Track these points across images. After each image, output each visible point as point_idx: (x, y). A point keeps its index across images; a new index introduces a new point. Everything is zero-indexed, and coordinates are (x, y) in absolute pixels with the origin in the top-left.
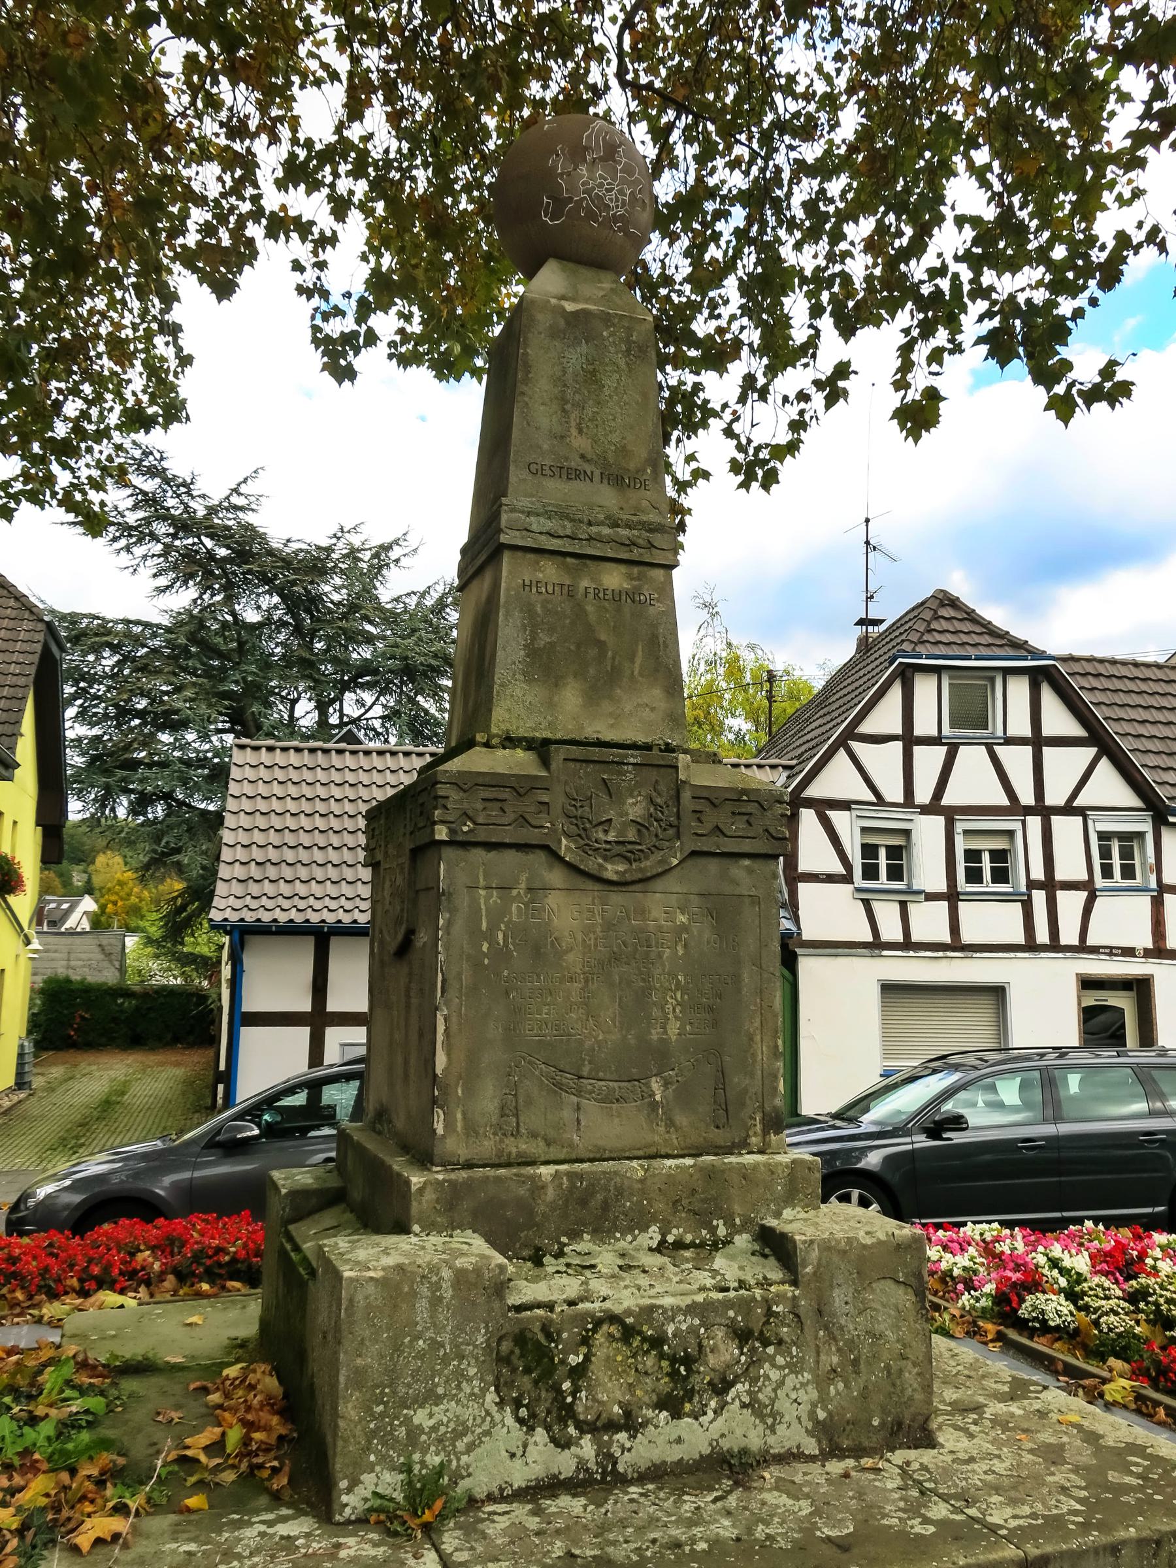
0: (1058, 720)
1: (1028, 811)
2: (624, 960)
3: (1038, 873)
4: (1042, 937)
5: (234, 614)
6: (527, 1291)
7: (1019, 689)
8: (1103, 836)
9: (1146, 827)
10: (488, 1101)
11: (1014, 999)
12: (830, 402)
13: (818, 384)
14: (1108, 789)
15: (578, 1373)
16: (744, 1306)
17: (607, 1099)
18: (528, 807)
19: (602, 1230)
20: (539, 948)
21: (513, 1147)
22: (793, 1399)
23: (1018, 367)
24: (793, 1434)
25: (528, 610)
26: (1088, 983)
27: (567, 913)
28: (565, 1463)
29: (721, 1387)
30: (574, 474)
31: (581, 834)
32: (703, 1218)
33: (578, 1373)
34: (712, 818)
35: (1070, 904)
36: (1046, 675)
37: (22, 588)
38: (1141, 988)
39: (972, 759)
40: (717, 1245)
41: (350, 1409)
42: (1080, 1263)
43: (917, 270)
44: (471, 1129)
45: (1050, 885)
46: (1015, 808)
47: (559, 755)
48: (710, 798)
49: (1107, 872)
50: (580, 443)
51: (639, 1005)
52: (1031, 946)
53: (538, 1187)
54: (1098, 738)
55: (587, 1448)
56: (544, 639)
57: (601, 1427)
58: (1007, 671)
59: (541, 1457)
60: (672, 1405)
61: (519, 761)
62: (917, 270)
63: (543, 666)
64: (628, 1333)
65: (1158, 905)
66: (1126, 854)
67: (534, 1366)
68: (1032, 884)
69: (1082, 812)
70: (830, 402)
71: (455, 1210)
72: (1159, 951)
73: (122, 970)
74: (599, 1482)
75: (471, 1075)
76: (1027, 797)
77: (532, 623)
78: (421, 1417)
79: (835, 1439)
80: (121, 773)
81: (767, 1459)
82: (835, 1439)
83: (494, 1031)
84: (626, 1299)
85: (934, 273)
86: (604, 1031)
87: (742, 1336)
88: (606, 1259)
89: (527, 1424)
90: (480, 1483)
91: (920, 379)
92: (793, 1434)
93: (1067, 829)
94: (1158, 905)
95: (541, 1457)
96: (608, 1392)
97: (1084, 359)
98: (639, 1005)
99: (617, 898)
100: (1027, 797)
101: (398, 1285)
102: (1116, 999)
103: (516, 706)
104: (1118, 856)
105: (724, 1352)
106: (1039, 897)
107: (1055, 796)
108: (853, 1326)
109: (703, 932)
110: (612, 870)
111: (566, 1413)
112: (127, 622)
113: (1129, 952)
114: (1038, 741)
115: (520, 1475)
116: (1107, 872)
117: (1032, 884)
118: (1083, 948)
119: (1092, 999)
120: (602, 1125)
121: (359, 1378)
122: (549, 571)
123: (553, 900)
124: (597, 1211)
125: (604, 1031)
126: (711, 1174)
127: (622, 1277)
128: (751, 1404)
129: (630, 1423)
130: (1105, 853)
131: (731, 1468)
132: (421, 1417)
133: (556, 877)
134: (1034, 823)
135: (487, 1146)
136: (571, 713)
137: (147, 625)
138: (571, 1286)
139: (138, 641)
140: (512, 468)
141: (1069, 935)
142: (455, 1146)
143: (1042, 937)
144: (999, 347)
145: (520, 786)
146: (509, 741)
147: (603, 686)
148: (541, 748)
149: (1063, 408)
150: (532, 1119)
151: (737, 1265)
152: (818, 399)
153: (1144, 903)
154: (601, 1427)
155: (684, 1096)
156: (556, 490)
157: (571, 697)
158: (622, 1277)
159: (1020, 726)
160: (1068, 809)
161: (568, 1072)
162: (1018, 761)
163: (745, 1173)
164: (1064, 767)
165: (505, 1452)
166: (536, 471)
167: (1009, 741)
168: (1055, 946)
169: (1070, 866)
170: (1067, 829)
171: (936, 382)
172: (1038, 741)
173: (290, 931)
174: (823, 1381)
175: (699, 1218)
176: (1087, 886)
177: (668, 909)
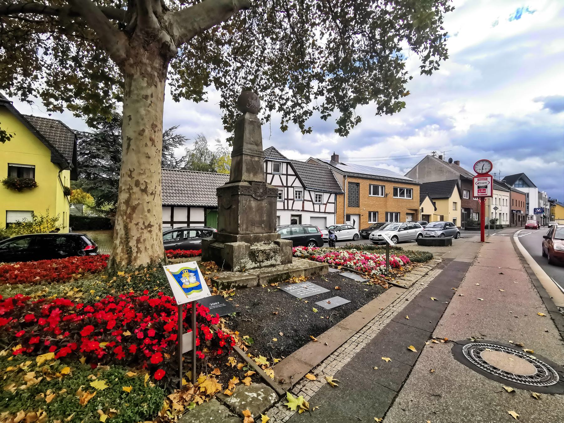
0: (290, 172)
1: (285, 187)
2: (260, 209)
3: (286, 197)
4: (286, 208)
5: (113, 133)
6: (251, 248)
7: (285, 165)
8: (296, 191)
9: (302, 190)
10: (244, 227)
11: (281, 218)
12: (267, 121)
13: (265, 118)
14: (297, 183)
15: (258, 256)
16: (274, 249)
17: (258, 227)
18: (249, 190)
19: (258, 242)
20: (250, 208)
21: (247, 232)
22: (279, 259)
23: (297, 124)
24: (279, 262)
25: (246, 163)
26: (292, 216)
27: (253, 204)
28: (256, 266)
29: (272, 258)
30: (251, 144)
31: (255, 193)
32: (268, 240)
33: (258, 256)
34: (270, 192)
35: (291, 202)
36: (289, 163)
37: (67, 125)
38: (300, 216)
39: (277, 177)
40: (270, 243)
41: (235, 260)
42: (301, 249)
43: (285, 107)
44: (243, 230)
45: (288, 199)
46: (283, 186)
47: (253, 183)
48: (270, 189)
49: (296, 197)
50: (252, 139)
51: (261, 216)
52: (284, 209)
53: (251, 237)
54: (296, 175)
55: (258, 264)
56: (248, 167)
57: (260, 262)
58: (283, 162)
59: (254, 265)
60: (267, 260)
61: (246, 184)
62: (285, 107)
63: (248, 171)
64: (263, 252)
65: (303, 202)
66: (299, 194)
67: (253, 255)
68: (285, 199)
69: (293, 187)
70: (267, 121)
71: (243, 239)
72: (303, 210)
73: (82, 213)
74: (260, 267)
75: (243, 224)
76: (285, 184)
77: (247, 165)
78: (242, 261)
79: (283, 263)
80: (85, 168)
81: (276, 265)
82: (283, 263)
83: (245, 218)
84: (262, 248)
85: (287, 108)
86: (257, 219)
87: (274, 252)
88: (258, 245)
89: (252, 262)
90: (248, 267)
91: (285, 124)
92: (279, 262)
93: (291, 190)
94: (303, 202)
95: (254, 265)
96: (261, 258)
97: (306, 125)
98: (261, 216)
99: (259, 202)
100: (285, 184)
101: (239, 247)
102: (297, 218)
103: (245, 176)
104: (298, 194)
105: (272, 254)
106: (286, 201)
107: (289, 185)
108: (285, 251)
109: (268, 206)
110: (259, 198)
111: (256, 260)
112: (84, 132)
113: (299, 210)
114: (287, 175)
115: (252, 267)
116: (296, 197)
117: (285, 199)
118: (292, 210)
119: (293, 218)
120: (257, 230)
121: (235, 256)
122: (249, 158)
123: (252, 202)
124: (257, 239)
125: (257, 219)
126: (269, 235)
127: (259, 246)
128: (275, 260)
129: (263, 262)
130: (296, 194)
131: (273, 266)
132: (242, 261)
133: (252, 199)
134: (286, 189)
135: (244, 232)
136: (252, 177)
137: (89, 133)
138: (256, 247)
139: (87, 137)
140: (244, 144)
141: (290, 208)
142: (241, 232)
143: (286, 208)
144: (295, 121)
145: (248, 187)
146: (245, 181)
147: (255, 174)
148: (250, 182)
149: (303, 132)
150: (249, 229)
151: (272, 245)
152: (265, 120)
153: (301, 202)
154: (260, 262)
155: (266, 226)
156: (250, 146)
157: (252, 175)
158: (259, 246)
159: (285, 172)
160: (291, 187)
161: (253, 224)
162: (283, 178)
163: (273, 235)
164: (291, 179)
165: (250, 264)
166: (247, 143)
167: (283, 174)
168: (288, 210)
169: (291, 197)
170: (291, 190)
171: (287, 125)
172: (287, 175)
173: (183, 206)
174: (282, 257)
175: (268, 240)
176: (293, 200)
177: (264, 204)
